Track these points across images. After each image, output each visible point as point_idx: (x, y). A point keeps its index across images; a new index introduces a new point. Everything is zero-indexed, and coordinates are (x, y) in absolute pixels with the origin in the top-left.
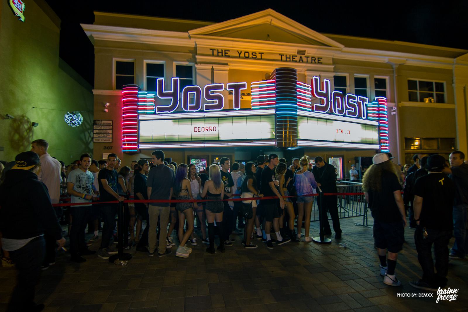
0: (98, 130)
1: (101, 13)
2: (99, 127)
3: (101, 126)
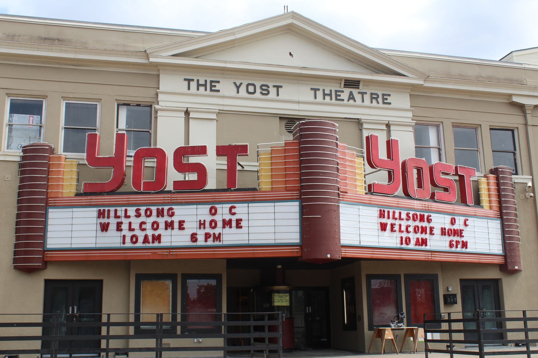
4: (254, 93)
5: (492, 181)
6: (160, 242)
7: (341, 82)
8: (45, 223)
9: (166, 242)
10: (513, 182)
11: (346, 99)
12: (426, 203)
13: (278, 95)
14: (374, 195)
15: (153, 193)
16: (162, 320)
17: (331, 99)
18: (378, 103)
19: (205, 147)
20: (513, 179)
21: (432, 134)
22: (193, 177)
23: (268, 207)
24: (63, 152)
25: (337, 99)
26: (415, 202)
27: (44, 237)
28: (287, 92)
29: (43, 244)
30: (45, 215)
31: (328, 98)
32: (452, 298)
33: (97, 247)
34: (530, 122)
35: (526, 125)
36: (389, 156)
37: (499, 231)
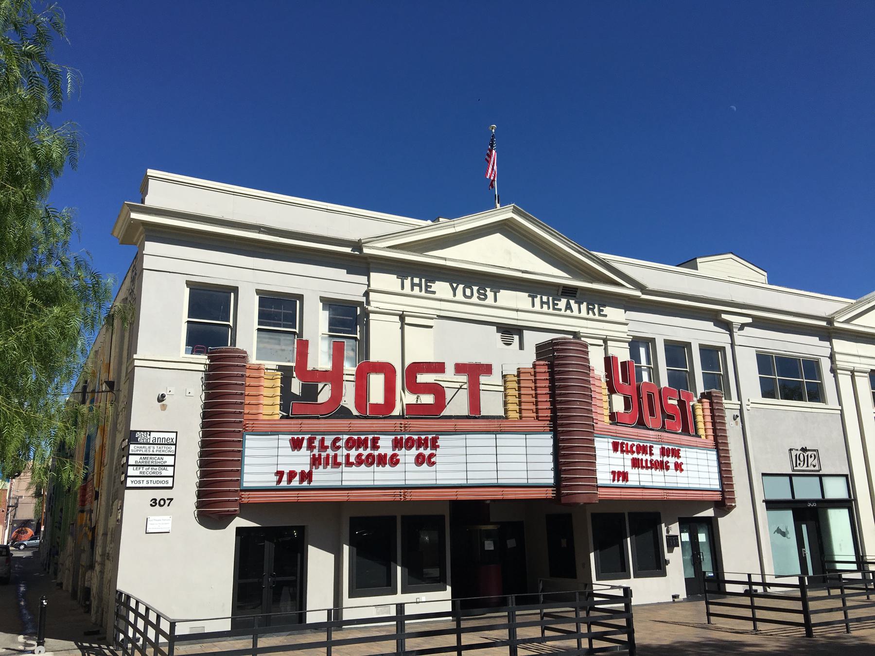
0: (140, 457)
1: (447, 552)
2: (145, 449)
3: (147, 446)
4: (470, 297)
6: (310, 481)
7: (559, 289)
8: (241, 453)
9: (633, 480)
11: (563, 309)
13: (496, 300)
15: (381, 418)
17: (549, 308)
18: (594, 314)
19: (491, 365)
21: (642, 351)
23: (518, 440)
24: (256, 360)
25: (427, 291)
26: (651, 432)
28: (507, 297)
29: (239, 482)
30: (241, 443)
31: (417, 289)
32: (27, 606)
33: (530, 484)
34: (737, 342)
35: (733, 345)
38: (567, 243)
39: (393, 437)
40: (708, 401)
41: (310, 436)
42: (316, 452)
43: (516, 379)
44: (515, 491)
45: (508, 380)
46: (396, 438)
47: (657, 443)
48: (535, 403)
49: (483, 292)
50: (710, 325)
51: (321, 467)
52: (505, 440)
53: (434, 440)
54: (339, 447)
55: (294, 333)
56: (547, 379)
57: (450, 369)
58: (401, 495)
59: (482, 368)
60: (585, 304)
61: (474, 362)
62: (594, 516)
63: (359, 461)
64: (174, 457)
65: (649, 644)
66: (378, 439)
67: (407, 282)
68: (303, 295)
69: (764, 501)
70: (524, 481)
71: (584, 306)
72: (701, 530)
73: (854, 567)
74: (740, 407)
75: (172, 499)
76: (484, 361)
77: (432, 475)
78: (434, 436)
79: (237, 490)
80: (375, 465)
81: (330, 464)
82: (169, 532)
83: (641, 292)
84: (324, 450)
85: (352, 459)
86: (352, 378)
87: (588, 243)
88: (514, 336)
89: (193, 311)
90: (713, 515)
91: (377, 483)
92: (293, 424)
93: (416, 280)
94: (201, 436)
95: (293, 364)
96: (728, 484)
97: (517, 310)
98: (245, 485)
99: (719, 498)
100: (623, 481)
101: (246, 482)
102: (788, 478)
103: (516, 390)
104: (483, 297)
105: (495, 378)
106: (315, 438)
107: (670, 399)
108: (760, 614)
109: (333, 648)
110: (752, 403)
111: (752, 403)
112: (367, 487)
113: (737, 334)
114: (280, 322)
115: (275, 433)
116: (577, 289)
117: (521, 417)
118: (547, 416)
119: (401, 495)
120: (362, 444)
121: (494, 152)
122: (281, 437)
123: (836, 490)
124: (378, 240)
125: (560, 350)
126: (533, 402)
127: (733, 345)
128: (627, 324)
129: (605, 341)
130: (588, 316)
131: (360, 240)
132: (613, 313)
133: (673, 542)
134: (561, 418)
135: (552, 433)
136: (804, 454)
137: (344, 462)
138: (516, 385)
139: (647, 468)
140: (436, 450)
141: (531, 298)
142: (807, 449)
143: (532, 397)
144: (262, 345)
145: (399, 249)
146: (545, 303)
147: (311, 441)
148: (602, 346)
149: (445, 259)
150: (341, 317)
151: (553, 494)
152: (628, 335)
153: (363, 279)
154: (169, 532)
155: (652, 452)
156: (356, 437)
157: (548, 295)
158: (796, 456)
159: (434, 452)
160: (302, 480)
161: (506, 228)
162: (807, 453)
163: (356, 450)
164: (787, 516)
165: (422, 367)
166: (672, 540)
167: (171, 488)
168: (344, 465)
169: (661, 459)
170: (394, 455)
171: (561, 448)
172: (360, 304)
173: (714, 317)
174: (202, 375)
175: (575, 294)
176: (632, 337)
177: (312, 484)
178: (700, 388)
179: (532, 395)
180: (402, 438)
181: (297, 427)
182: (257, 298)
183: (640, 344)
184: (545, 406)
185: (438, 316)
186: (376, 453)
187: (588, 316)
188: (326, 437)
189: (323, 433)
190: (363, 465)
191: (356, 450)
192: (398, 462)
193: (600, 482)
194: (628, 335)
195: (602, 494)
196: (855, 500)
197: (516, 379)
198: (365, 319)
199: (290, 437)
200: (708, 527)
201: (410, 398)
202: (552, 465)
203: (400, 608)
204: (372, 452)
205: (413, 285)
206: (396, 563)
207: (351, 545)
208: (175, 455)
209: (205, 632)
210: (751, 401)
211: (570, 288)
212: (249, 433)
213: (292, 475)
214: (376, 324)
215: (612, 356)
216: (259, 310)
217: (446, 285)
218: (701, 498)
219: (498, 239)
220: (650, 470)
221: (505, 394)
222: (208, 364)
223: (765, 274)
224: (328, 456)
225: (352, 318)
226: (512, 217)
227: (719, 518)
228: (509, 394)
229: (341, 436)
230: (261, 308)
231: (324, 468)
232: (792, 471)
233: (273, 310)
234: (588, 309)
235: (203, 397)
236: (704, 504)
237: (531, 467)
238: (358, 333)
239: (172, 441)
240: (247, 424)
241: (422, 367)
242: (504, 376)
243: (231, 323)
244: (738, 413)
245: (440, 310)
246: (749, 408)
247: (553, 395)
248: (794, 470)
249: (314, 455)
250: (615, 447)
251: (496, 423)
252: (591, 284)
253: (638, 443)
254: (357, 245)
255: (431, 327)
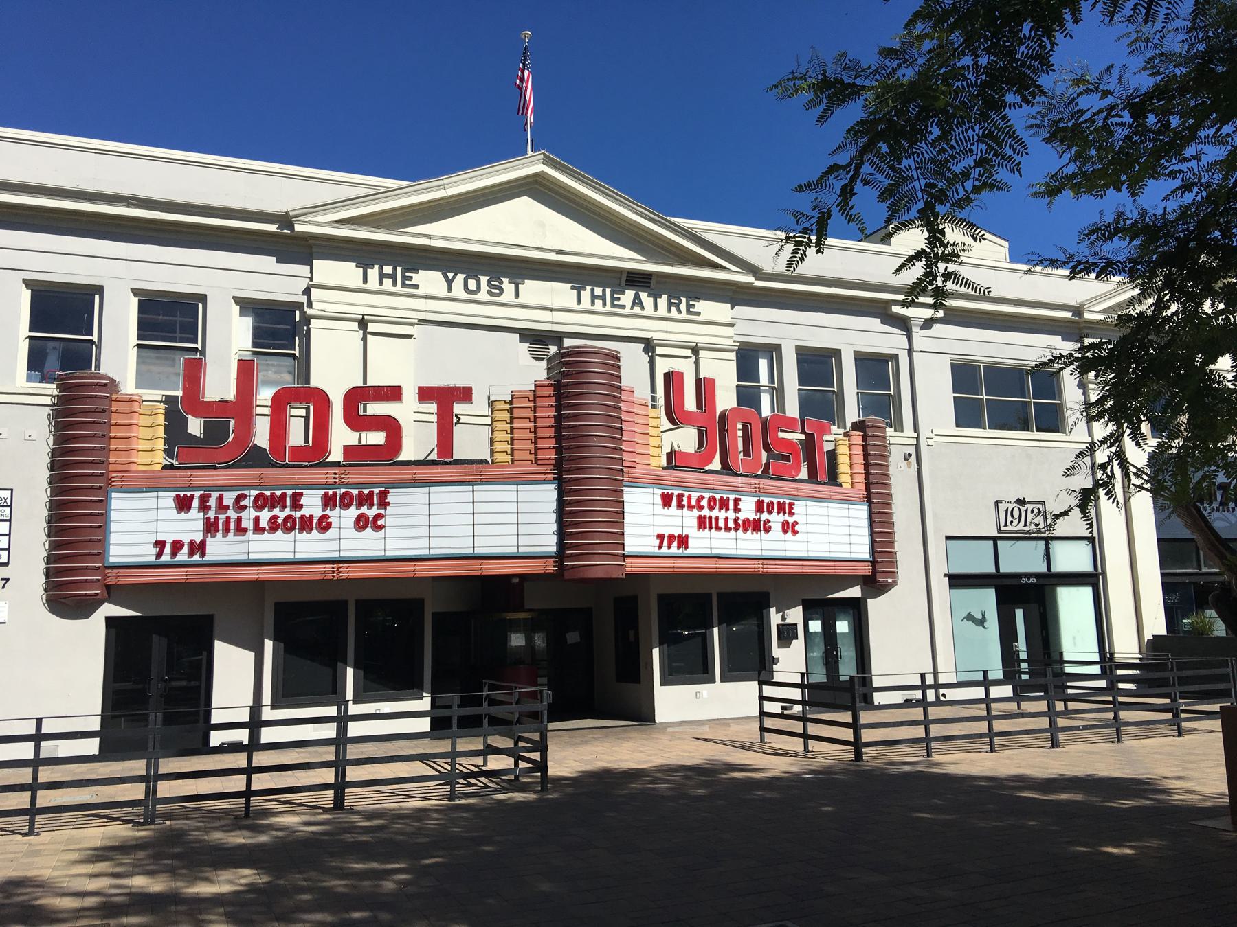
5: (857, 438)
6: (203, 554)
8: (104, 517)
10: (888, 442)
12: (757, 481)
13: (517, 295)
14: (676, 470)
15: (306, 466)
16: (348, 712)
18: (679, 311)
20: (888, 438)
21: (763, 364)
22: (376, 438)
23: (506, 493)
26: (740, 479)
27: (103, 543)
28: (534, 290)
29: (102, 555)
30: (105, 503)
31: (599, 303)
35: (910, 351)
36: (699, 406)
37: (865, 523)
38: (631, 207)
39: (323, 492)
40: (861, 434)
41: (202, 492)
42: (212, 514)
43: (508, 406)
44: (504, 563)
45: (496, 408)
46: (326, 494)
47: (749, 494)
48: (533, 441)
49: (497, 284)
50: (875, 323)
51: (219, 535)
52: (485, 493)
53: (383, 496)
54: (245, 507)
55: (196, 350)
56: (552, 406)
57: (410, 394)
58: (333, 572)
59: (457, 394)
60: (665, 297)
61: (446, 384)
62: (662, 598)
63: (274, 526)
64: (8, 523)
65: (1089, 775)
66: (301, 494)
67: (373, 273)
68: (206, 295)
69: (945, 576)
70: (513, 550)
71: (663, 301)
72: (842, 616)
73: (1096, 670)
74: (917, 442)
75: (7, 580)
76: (460, 382)
77: (380, 544)
78: (383, 489)
79: (99, 567)
80: (297, 531)
81: (221, 532)
82: (5, 623)
83: (753, 276)
84: (224, 511)
85: (264, 523)
86: (267, 411)
87: (663, 206)
88: (550, 347)
89: (37, 321)
90: (860, 596)
91: (299, 556)
92: (180, 476)
93: (598, 291)
94: (49, 495)
95: (180, 393)
96: (882, 552)
97: (552, 310)
98: (112, 560)
99: (867, 571)
100: (679, 547)
101: (112, 556)
102: (992, 542)
103: (507, 423)
104: (497, 291)
105: (479, 406)
106: (209, 496)
107: (782, 431)
108: (813, 729)
109: (254, 776)
110: (936, 435)
111: (936, 435)
112: (284, 561)
113: (919, 334)
114: (175, 335)
115: (154, 490)
116: (651, 275)
117: (513, 461)
118: (550, 459)
119: (333, 572)
120: (280, 502)
121: (526, 72)
122: (161, 494)
123: (1071, 558)
124: (317, 212)
125: (570, 364)
126: (531, 440)
127: (910, 351)
128: (733, 325)
129: (695, 350)
130: (669, 315)
131: (287, 212)
132: (708, 309)
133: (788, 632)
134: (568, 460)
135: (557, 481)
136: (1021, 507)
137: (252, 527)
138: (507, 416)
139: (728, 529)
140: (386, 509)
141: (576, 291)
142: (1027, 500)
143: (530, 432)
144: (144, 368)
145: (358, 224)
146: (598, 297)
147: (204, 499)
148: (690, 357)
149: (429, 237)
150: (274, 326)
151: (554, 566)
152: (734, 341)
153: (304, 270)
154: (5, 623)
155: (739, 507)
156: (268, 493)
157: (604, 285)
158: (1007, 510)
159: (382, 511)
160: (191, 553)
161: (536, 188)
162: (1026, 506)
163: (269, 511)
164: (986, 601)
165: (367, 393)
166: (788, 630)
167: (6, 564)
168: (251, 532)
169: (757, 517)
170: (324, 518)
171: (567, 502)
172: (300, 306)
173: (881, 311)
174: (47, 411)
175: (650, 283)
176: (738, 344)
177: (206, 558)
178: (852, 414)
179: (530, 429)
180: (335, 494)
181: (184, 481)
182: (135, 301)
183: (760, 353)
184: (548, 444)
185: (420, 320)
186: (298, 514)
187: (668, 315)
188: (225, 493)
189: (221, 488)
190: (279, 532)
191: (269, 511)
192: (329, 526)
193: (628, 550)
194: (734, 341)
195: (633, 566)
196: (1104, 573)
197: (508, 406)
198: (305, 328)
199: (174, 494)
200: (853, 613)
201: (352, 438)
202: (554, 527)
203: (154, 718)
204: (293, 513)
205: (594, 297)
206: (346, 664)
207: (275, 639)
208: (10, 520)
209: (59, 756)
210: (935, 433)
211: (638, 274)
212: (116, 490)
213: (177, 546)
214: (320, 334)
215: (672, 372)
216: (139, 317)
217: (438, 275)
218: (752, 570)
219: (525, 204)
220: (732, 532)
221: (492, 428)
222: (57, 396)
223: (1006, 244)
224: (228, 519)
225: (289, 327)
226: (543, 171)
227: (868, 600)
228: (496, 429)
229: (247, 492)
230: (141, 316)
231: (223, 537)
232: (999, 533)
233: (161, 317)
234: (670, 305)
235: (51, 442)
236: (847, 580)
237: (152, 515)
238: (297, 348)
239: (5, 501)
240: (114, 477)
241: (367, 393)
242: (492, 403)
243: (95, 338)
244: (912, 450)
245: (426, 311)
246: (931, 442)
247: (558, 429)
248: (1000, 531)
249: (208, 519)
250: (666, 500)
251: (474, 469)
252: (671, 267)
253: (711, 494)
254: (285, 220)
255: (410, 337)
